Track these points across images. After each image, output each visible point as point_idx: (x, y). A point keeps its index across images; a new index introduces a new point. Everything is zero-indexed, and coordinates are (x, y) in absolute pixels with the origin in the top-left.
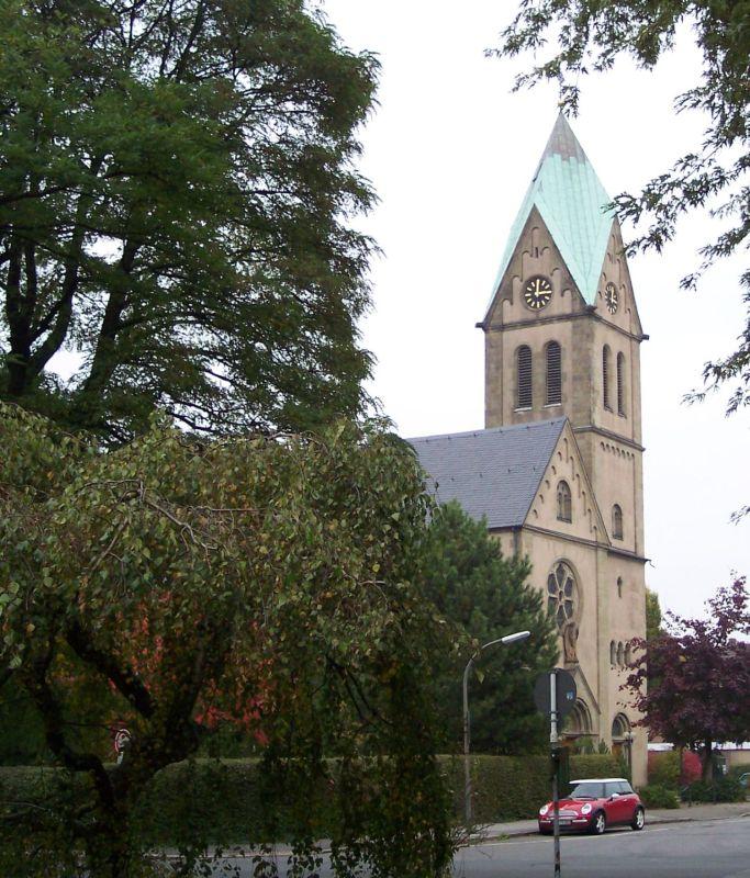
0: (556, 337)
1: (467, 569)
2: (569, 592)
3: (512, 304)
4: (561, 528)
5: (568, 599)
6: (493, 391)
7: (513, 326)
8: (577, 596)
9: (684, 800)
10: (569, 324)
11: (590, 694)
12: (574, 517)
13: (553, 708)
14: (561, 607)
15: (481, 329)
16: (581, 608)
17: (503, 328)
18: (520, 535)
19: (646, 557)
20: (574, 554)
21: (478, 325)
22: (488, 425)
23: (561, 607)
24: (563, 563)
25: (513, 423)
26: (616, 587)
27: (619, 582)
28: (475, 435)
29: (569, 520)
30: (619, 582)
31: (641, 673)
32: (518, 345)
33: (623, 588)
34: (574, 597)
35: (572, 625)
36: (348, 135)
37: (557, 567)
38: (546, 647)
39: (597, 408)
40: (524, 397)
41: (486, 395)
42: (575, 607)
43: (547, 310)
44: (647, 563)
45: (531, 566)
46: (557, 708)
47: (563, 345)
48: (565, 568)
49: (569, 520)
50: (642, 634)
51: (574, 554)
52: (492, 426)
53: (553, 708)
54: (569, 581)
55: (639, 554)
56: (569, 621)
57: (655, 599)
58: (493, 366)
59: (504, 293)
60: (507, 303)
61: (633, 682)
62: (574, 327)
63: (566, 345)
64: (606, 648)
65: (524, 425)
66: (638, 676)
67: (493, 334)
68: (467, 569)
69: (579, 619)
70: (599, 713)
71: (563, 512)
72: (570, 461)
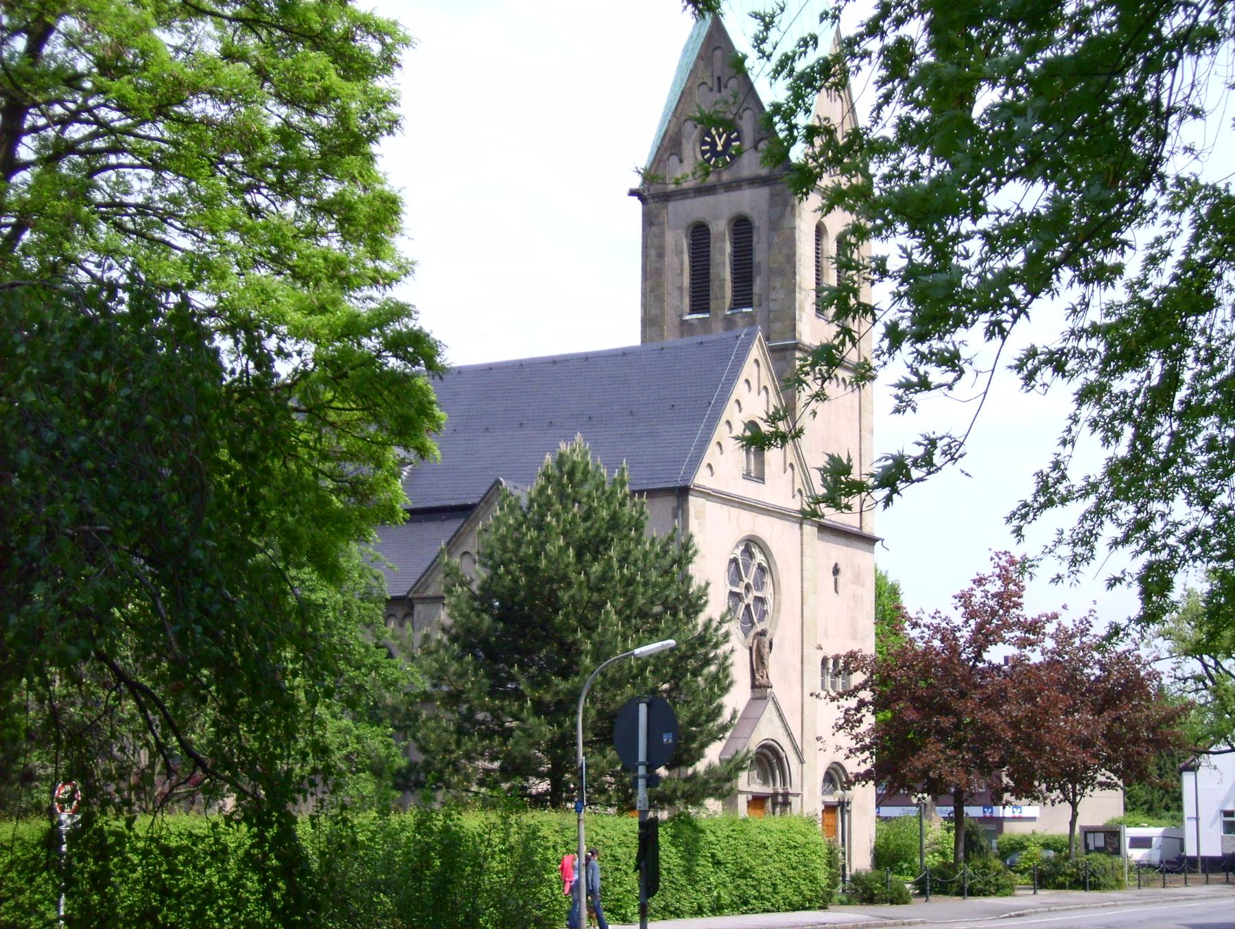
0: (746, 209)
1: (591, 547)
2: (760, 585)
3: (681, 161)
4: (749, 490)
5: (759, 594)
6: (652, 290)
7: (683, 194)
8: (771, 590)
9: (923, 893)
10: (764, 192)
11: (790, 735)
12: (767, 476)
13: (642, 757)
14: (748, 607)
15: (636, 198)
16: (777, 609)
17: (666, 197)
18: (686, 500)
19: (877, 535)
20: (766, 528)
21: (633, 193)
22: (643, 342)
23: (748, 607)
24: (751, 544)
25: (682, 335)
26: (832, 578)
27: (836, 571)
28: (624, 353)
29: (761, 478)
30: (836, 571)
31: (862, 704)
32: (689, 221)
33: (840, 578)
34: (767, 593)
35: (763, 633)
36: (1054, 199)
37: (741, 548)
38: (713, 668)
39: (805, 316)
40: (701, 299)
41: (644, 294)
42: (769, 607)
43: (734, 168)
44: (878, 544)
45: (696, 552)
46: (648, 757)
47: (757, 223)
48: (755, 551)
49: (761, 478)
50: (868, 646)
51: (766, 528)
52: (652, 340)
53: (642, 757)
54: (761, 568)
55: (867, 530)
56: (759, 627)
57: (894, 592)
58: (653, 252)
59: (669, 145)
60: (674, 159)
61: (849, 721)
62: (772, 196)
63: (760, 223)
64: (814, 667)
65: (696, 339)
66: (858, 709)
67: (652, 205)
68: (591, 547)
69: (775, 621)
70: (802, 762)
71: (752, 467)
72: (763, 393)
